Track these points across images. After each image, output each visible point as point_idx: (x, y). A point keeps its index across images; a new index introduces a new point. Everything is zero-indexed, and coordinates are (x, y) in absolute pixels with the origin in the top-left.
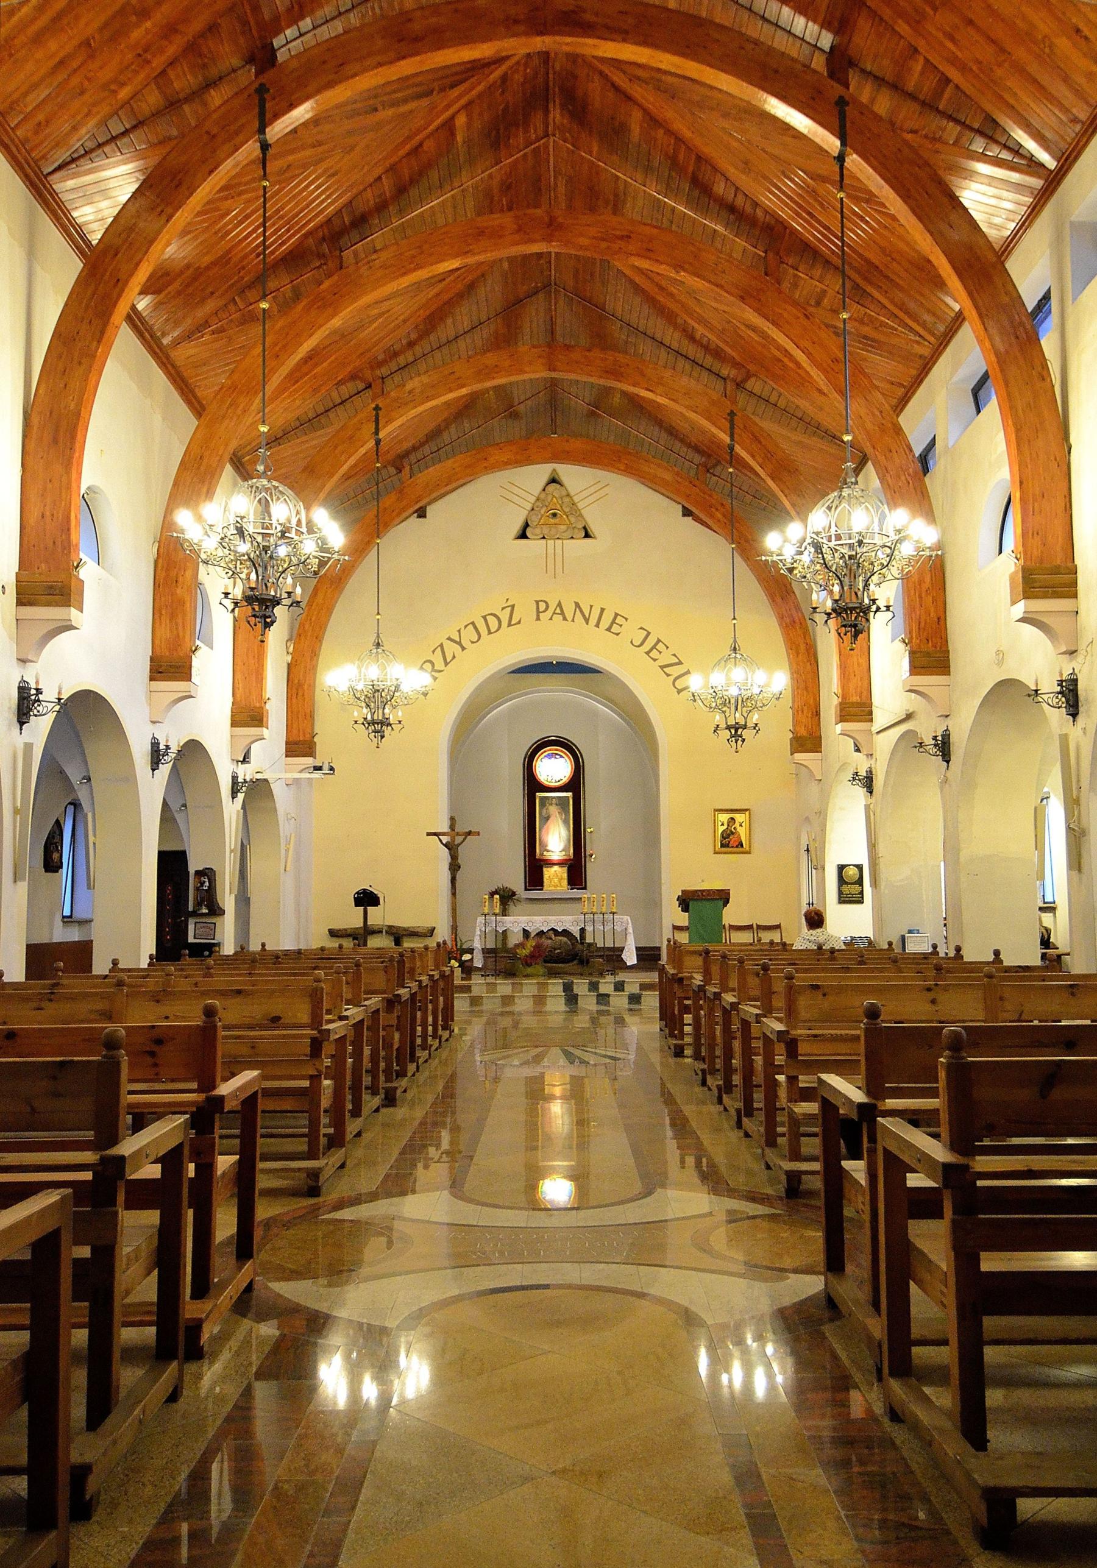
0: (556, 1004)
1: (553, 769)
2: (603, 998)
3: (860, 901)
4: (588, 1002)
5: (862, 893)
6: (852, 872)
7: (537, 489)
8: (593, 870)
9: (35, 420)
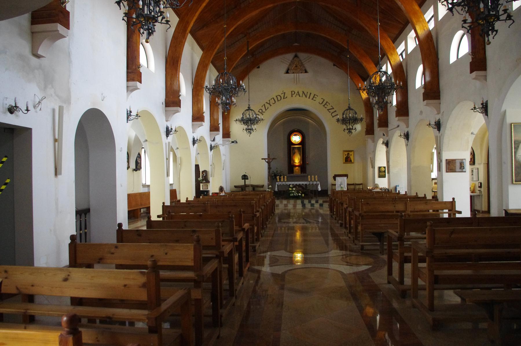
0: (299, 206)
1: (296, 139)
2: (312, 205)
3: (385, 177)
4: (308, 206)
5: (385, 175)
6: (383, 169)
7: (291, 58)
8: (308, 168)
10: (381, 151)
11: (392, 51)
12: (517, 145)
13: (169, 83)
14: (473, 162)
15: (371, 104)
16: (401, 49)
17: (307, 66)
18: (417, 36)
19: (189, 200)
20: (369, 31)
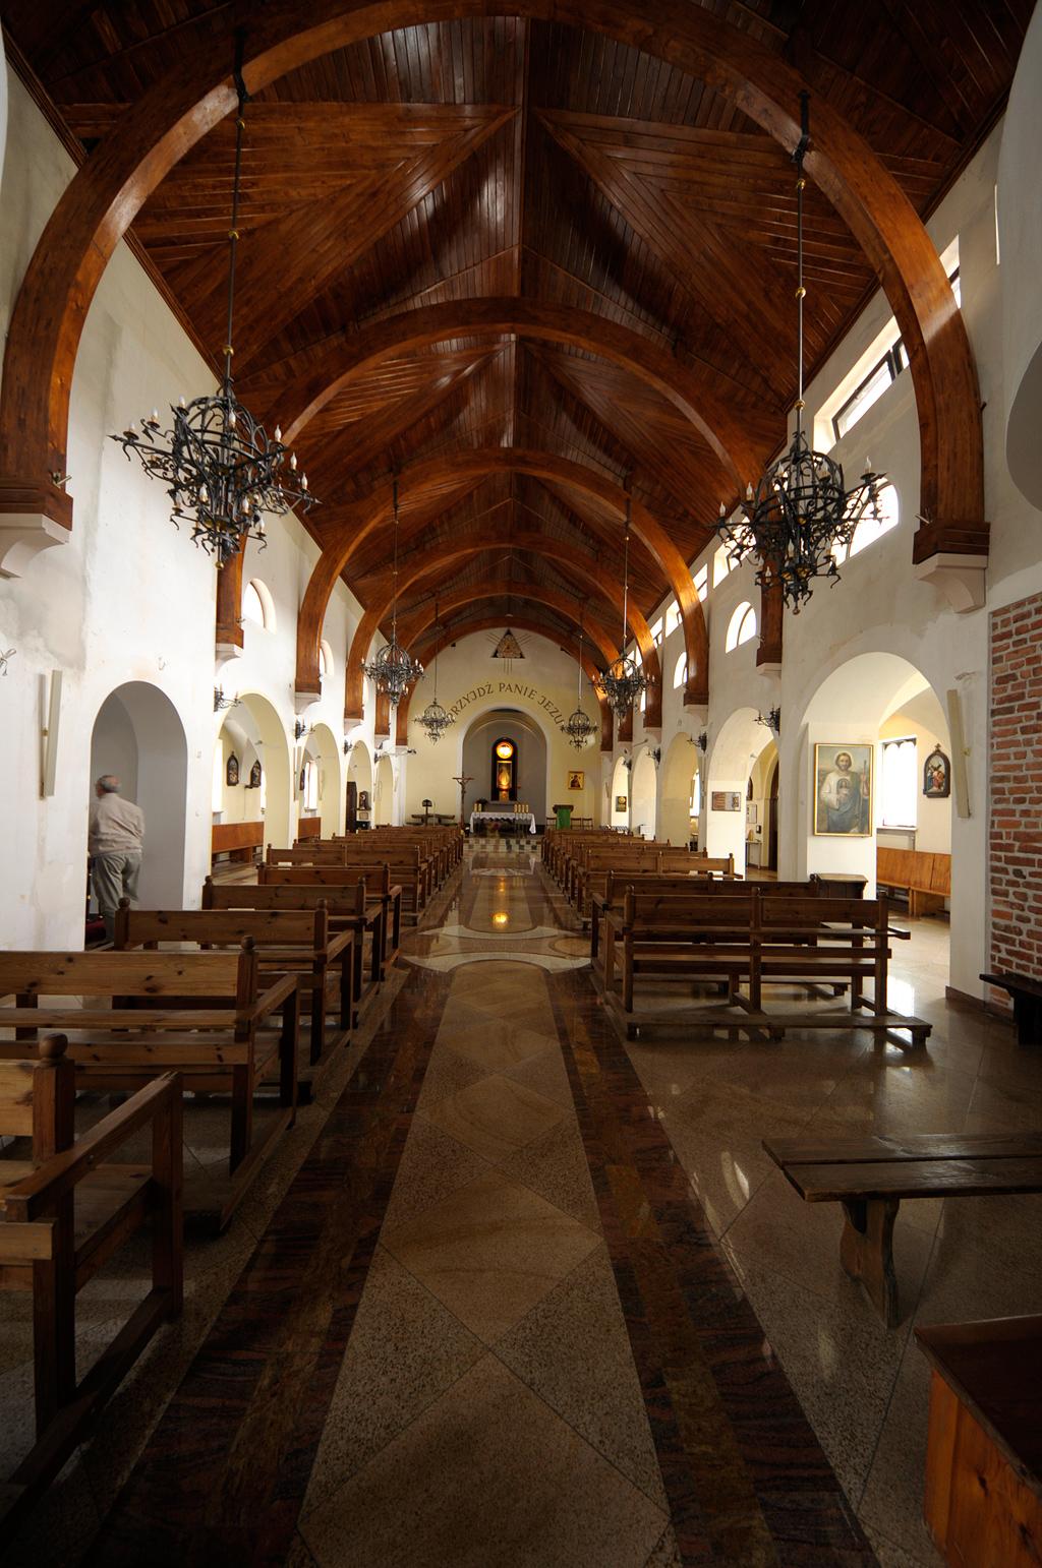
0: (503, 848)
1: (505, 752)
2: (521, 847)
4: (516, 848)
8: (520, 793)
9: (302, 617)
10: (621, 772)
11: (643, 632)
12: (821, 778)
13: (302, 655)
14: (750, 797)
15: (609, 707)
17: (524, 649)
18: (681, 611)
19: (272, 848)
20: (614, 602)
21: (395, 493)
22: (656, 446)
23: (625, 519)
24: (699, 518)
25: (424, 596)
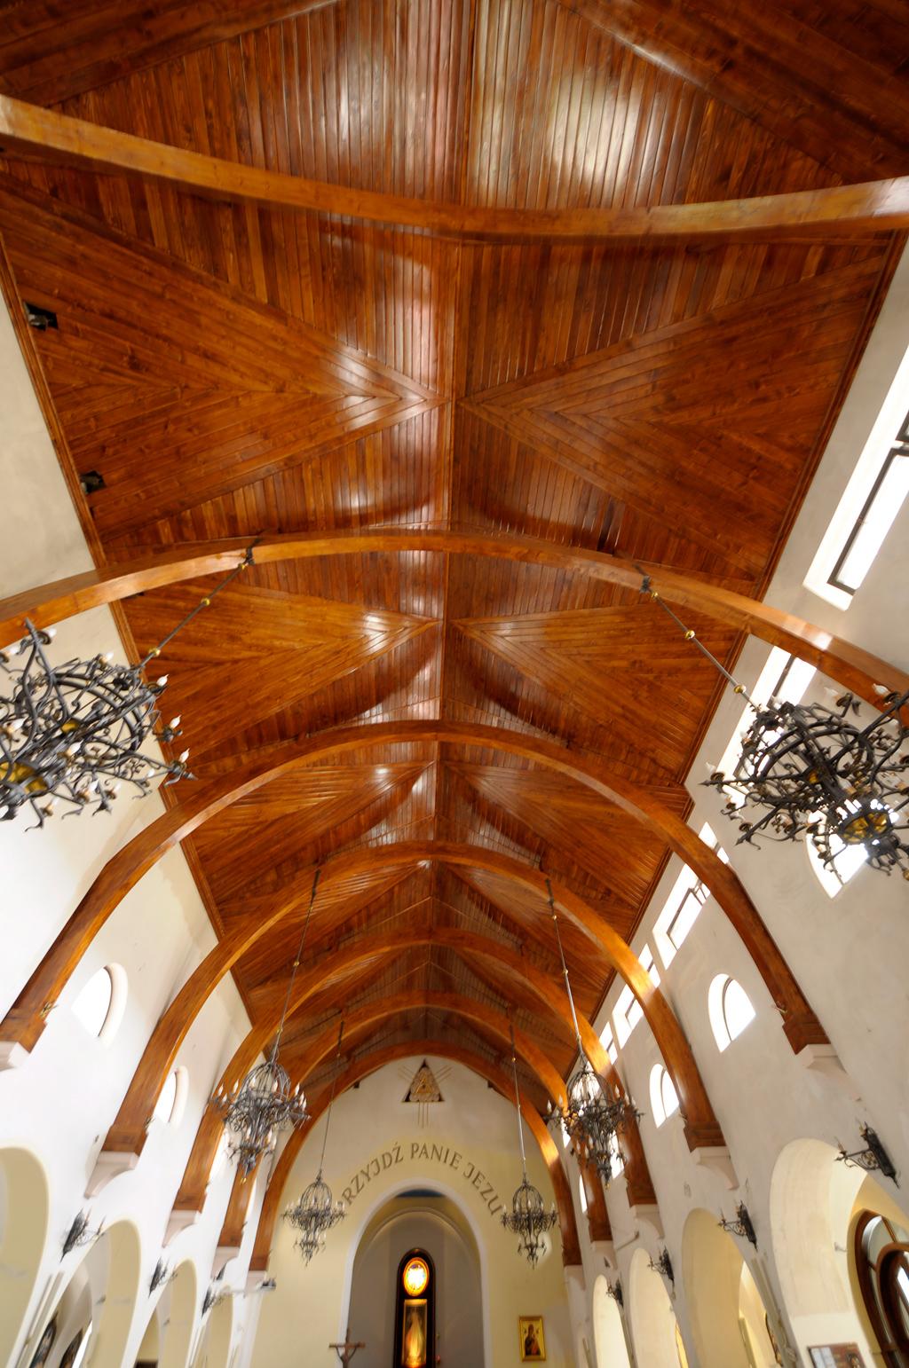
1: (416, 1279)
9: (161, 1026)
13: (139, 1083)
16: (605, 1037)
17: (444, 1087)
21: (316, 881)
22: (566, 828)
23: (547, 898)
24: (622, 895)
25: (330, 1013)
